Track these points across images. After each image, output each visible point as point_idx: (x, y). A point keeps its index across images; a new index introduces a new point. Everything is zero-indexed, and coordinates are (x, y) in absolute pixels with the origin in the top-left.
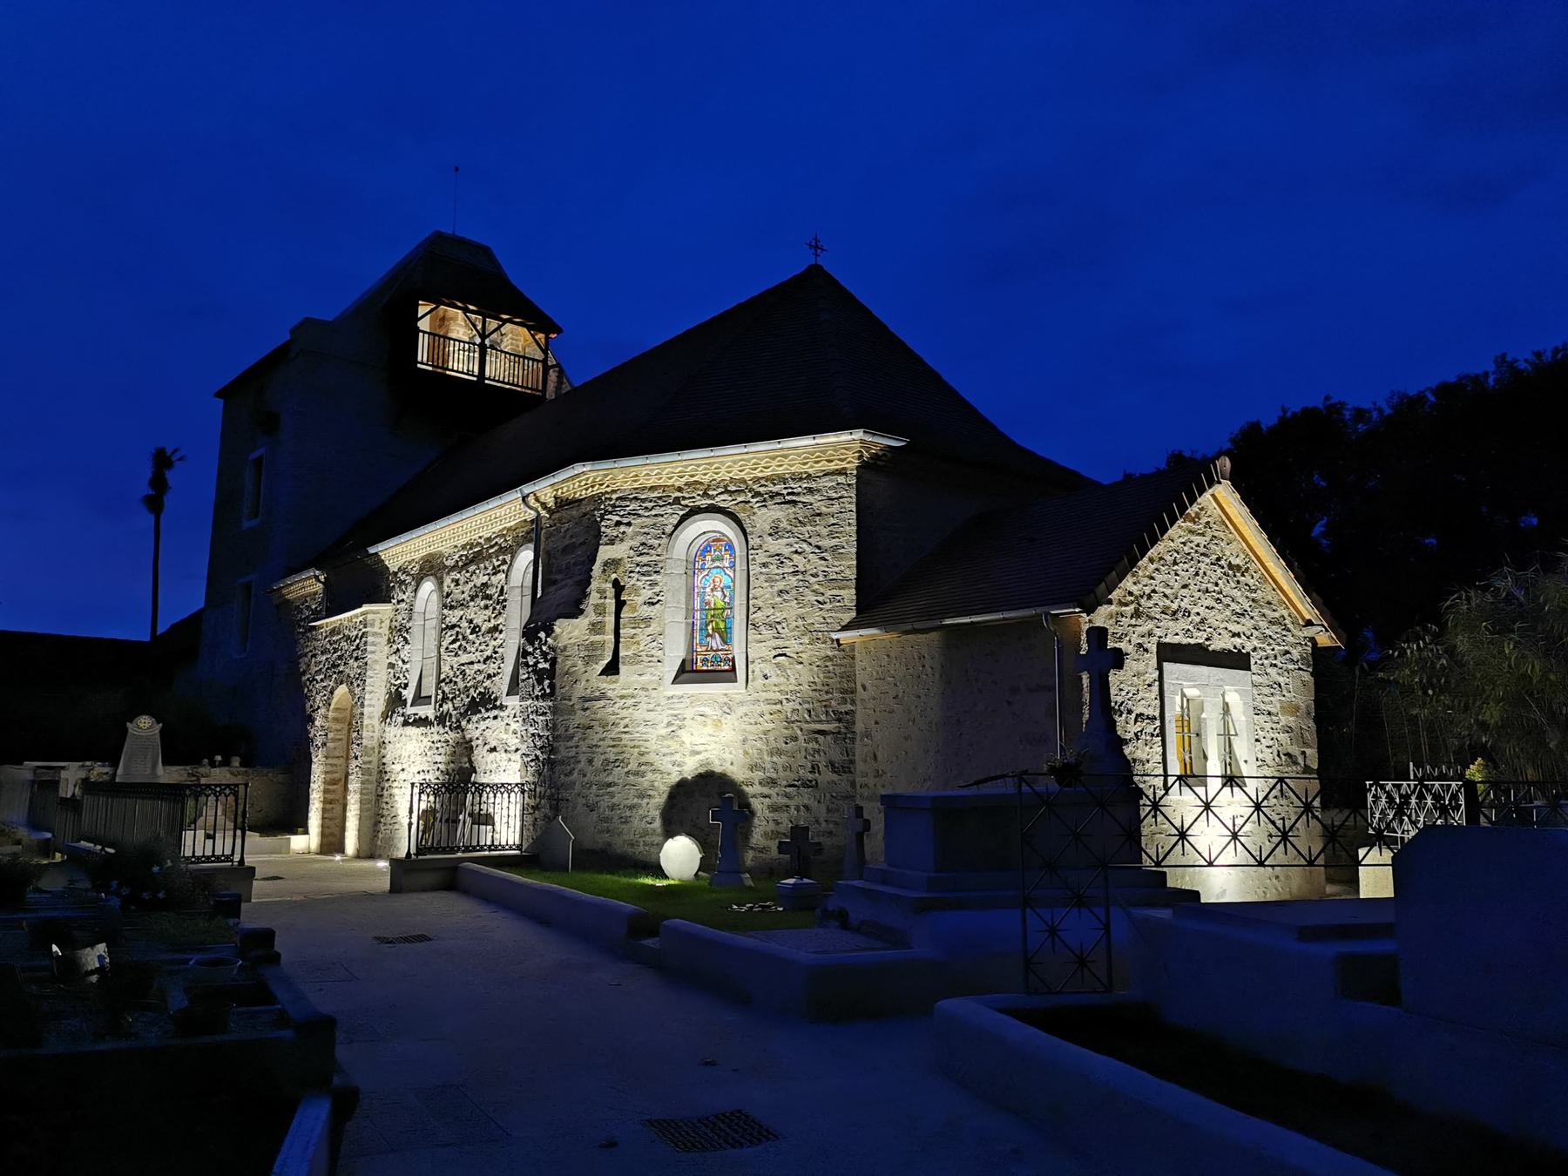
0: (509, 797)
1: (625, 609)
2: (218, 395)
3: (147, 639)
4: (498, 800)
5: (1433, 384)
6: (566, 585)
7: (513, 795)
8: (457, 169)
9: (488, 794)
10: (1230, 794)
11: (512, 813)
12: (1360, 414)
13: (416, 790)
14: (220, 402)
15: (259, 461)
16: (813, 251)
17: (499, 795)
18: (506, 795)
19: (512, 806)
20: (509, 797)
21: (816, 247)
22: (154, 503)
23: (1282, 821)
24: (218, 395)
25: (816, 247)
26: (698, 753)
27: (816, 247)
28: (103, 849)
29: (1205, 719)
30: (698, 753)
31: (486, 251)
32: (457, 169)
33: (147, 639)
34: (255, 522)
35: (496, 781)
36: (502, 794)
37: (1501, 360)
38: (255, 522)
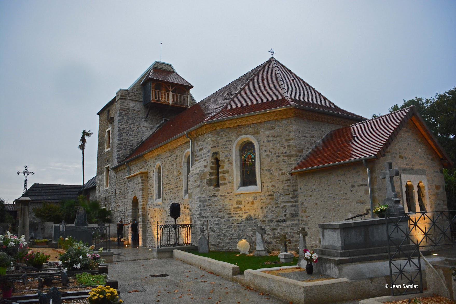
0: (187, 229)
1: (220, 167)
2: (98, 114)
3: (82, 185)
4: (184, 229)
5: (447, 90)
6: (201, 161)
7: (188, 228)
8: (161, 43)
9: (181, 228)
10: (416, 217)
11: (189, 233)
12: (427, 101)
13: (159, 227)
14: (98, 116)
15: (109, 132)
16: (273, 51)
17: (184, 228)
18: (186, 228)
19: (188, 231)
20: (187, 229)
21: (272, 52)
22: (82, 147)
23: (327, 232)
24: (98, 114)
25: (272, 52)
26: (247, 212)
27: (272, 52)
28: (109, 251)
29: (414, 192)
30: (247, 212)
31: (170, 65)
32: (161, 43)
33: (82, 185)
34: (109, 149)
35: (183, 224)
36: (185, 227)
37: (437, 94)
38: (109, 149)
